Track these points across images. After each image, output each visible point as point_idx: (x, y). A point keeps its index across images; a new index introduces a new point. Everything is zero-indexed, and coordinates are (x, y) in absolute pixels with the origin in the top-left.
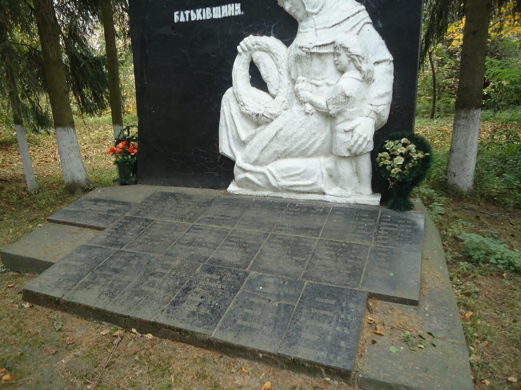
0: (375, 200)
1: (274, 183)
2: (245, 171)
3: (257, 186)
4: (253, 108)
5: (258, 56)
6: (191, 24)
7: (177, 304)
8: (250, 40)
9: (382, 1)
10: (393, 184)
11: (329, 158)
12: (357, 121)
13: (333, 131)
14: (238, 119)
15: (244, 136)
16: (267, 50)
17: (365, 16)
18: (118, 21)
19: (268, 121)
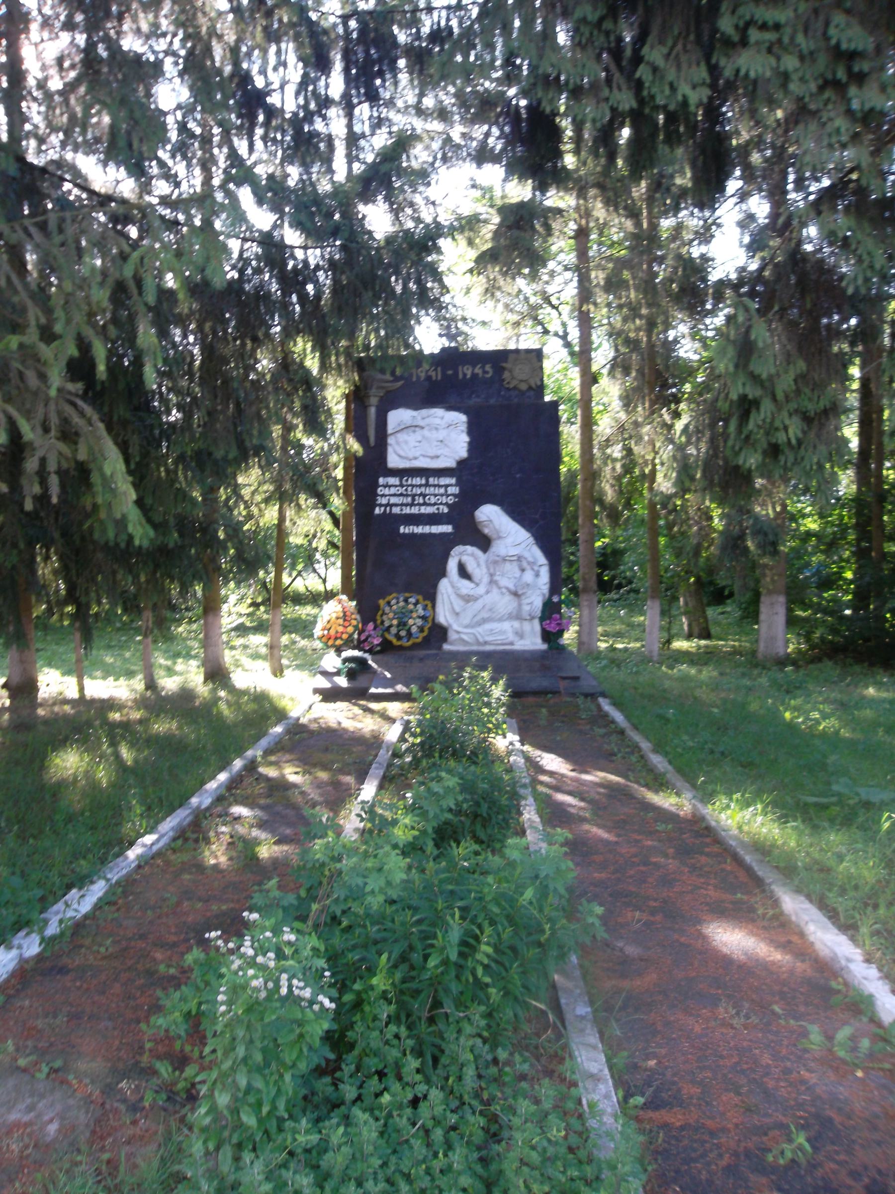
0: (544, 647)
1: (481, 640)
2: (458, 632)
3: (465, 643)
4: (464, 591)
5: (465, 559)
6: (413, 536)
7: (463, 222)
8: (459, 549)
9: (893, 271)
10: (265, 616)
11: (95, 637)
12: (533, 598)
13: (520, 605)
14: (453, 597)
15: (457, 609)
16: (472, 555)
17: (531, 540)
18: (78, 110)
19: (476, 599)
